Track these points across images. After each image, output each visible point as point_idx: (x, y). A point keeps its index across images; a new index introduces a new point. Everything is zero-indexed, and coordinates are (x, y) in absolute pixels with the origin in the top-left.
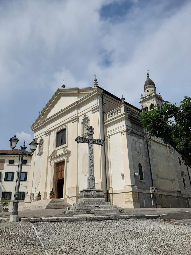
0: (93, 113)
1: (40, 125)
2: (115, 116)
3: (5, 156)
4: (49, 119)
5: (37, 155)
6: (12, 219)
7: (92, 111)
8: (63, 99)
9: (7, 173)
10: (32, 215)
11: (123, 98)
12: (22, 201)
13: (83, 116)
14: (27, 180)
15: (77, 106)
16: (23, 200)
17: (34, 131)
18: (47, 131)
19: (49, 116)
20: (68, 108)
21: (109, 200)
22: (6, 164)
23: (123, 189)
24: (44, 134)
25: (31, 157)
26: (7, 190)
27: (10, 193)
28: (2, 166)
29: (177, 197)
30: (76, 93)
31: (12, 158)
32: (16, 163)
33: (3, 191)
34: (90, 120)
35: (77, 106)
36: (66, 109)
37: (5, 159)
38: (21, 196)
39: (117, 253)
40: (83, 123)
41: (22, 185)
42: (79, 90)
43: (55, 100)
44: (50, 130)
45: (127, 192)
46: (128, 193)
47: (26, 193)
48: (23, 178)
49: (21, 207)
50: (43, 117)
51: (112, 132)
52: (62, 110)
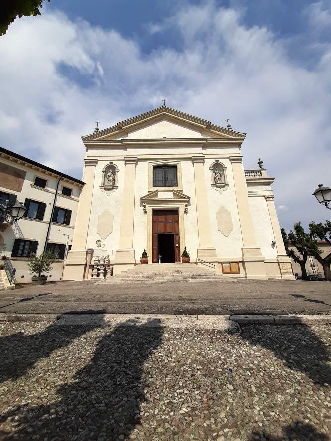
0: (127, 164)
1: (238, 140)
2: (254, 177)
3: (28, 166)
4: (127, 140)
7: (126, 161)
11: (261, 161)
12: (58, 262)
13: (108, 163)
14: (71, 224)
16: (60, 260)
17: (86, 145)
18: (127, 157)
19: (132, 136)
20: (172, 139)
21: (20, 253)
22: (27, 183)
24: (123, 158)
25: (81, 187)
26: (28, 237)
27: (34, 245)
29: (240, 265)
30: (202, 128)
31: (42, 176)
32: (50, 187)
33: (18, 237)
36: (141, 141)
37: (26, 172)
38: (57, 251)
41: (273, 245)
42: (209, 125)
43: (151, 119)
44: (139, 157)
45: (284, 262)
46: (285, 264)
47: (67, 248)
48: (61, 218)
50: (118, 133)
52: (165, 139)
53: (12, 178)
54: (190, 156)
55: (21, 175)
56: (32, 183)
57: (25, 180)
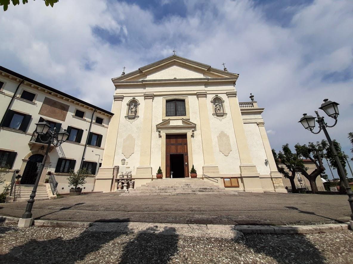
4: (146, 81)
5: (123, 120)
6: (317, 185)
7: (145, 97)
8: (175, 67)
9: (70, 129)
10: (226, 191)
12: (91, 177)
13: (132, 98)
15: (205, 83)
16: (92, 175)
18: (146, 93)
19: (150, 77)
20: (181, 80)
22: (70, 115)
23: (268, 174)
25: (111, 117)
27: (72, 162)
28: (62, 116)
30: (204, 71)
34: (139, 105)
35: (205, 83)
39: (54, 262)
40: (129, 105)
42: (209, 69)
43: (165, 65)
44: (155, 94)
45: (276, 178)
48: (94, 141)
49: (87, 185)
51: (246, 121)
52: (175, 79)
53: (58, 110)
54: (195, 92)
55: (65, 109)
56: (74, 114)
57: (68, 112)
